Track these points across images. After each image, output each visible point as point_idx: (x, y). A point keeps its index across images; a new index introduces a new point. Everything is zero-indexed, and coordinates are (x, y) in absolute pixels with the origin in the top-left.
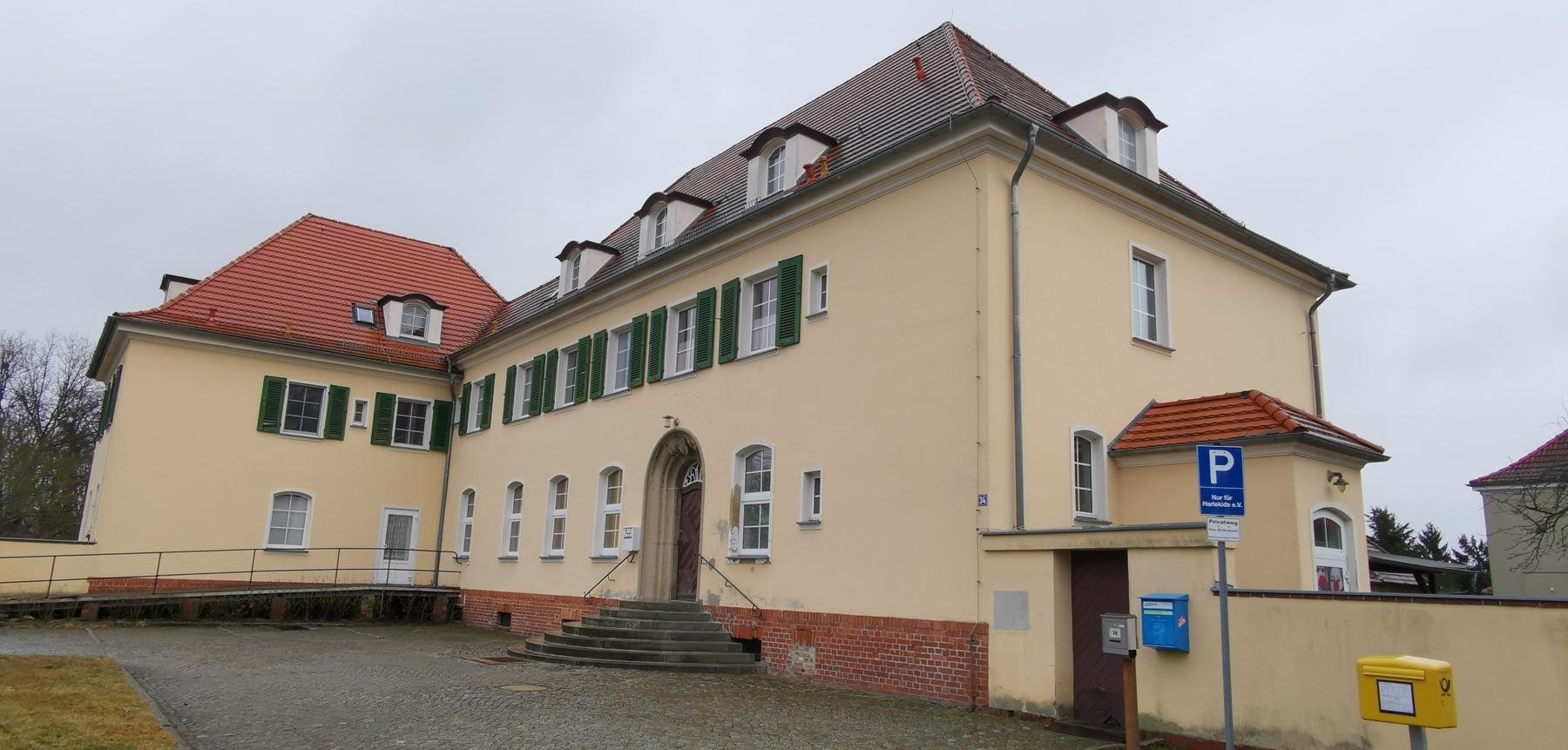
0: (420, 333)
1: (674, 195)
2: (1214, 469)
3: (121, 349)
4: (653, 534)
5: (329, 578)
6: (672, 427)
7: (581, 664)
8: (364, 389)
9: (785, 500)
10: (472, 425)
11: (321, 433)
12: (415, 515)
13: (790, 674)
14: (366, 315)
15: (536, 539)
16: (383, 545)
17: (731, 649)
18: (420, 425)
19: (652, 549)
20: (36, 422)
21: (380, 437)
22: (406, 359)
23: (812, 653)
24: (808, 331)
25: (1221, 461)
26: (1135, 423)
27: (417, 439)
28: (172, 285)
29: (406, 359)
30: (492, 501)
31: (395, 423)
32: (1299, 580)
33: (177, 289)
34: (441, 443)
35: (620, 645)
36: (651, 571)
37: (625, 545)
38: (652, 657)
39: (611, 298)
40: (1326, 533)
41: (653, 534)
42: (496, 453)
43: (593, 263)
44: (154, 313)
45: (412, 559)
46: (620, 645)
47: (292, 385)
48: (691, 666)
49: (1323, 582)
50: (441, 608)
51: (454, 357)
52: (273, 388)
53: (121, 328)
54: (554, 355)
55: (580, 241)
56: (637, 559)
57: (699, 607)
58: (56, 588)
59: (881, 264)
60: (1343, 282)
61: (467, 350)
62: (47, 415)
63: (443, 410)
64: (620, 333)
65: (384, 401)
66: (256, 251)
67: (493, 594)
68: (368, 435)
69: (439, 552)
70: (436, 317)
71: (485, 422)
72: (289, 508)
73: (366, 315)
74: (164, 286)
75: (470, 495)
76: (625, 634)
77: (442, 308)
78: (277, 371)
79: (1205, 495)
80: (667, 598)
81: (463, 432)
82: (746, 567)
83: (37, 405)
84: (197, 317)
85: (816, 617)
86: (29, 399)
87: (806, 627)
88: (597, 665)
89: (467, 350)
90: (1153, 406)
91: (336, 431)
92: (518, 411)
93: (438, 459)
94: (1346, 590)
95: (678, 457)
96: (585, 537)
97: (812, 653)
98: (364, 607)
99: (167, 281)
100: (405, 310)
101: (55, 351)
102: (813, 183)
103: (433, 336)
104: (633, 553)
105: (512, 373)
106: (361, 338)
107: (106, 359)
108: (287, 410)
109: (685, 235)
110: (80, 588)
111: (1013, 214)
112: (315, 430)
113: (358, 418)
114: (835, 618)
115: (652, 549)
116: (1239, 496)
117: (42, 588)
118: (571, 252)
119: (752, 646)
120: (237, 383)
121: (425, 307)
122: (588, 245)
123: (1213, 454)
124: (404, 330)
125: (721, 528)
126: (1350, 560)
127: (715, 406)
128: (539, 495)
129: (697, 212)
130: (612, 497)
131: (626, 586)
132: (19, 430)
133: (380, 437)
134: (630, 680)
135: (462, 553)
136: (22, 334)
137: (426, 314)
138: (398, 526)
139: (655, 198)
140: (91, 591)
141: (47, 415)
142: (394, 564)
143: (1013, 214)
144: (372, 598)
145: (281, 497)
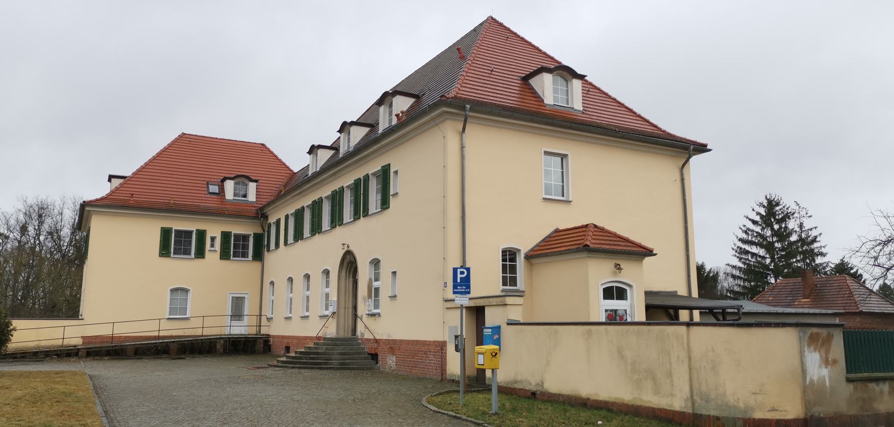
0: (245, 196)
1: (395, 92)
2: (459, 276)
3: (88, 220)
4: (342, 303)
5: (199, 332)
6: (346, 249)
7: (293, 368)
8: (214, 230)
9: (384, 284)
10: (272, 246)
11: (193, 256)
12: (246, 296)
13: (387, 370)
14: (214, 189)
15: (299, 310)
16: (230, 313)
17: (366, 358)
18: (246, 247)
19: (342, 311)
20: (59, 249)
21: (225, 255)
22: (236, 212)
23: (394, 358)
24: (393, 202)
25: (462, 273)
26: (543, 241)
27: (245, 255)
28: (113, 180)
29: (236, 212)
30: (282, 285)
31: (232, 248)
32: (589, 317)
33: (116, 182)
34: (258, 256)
35: (313, 358)
36: (342, 324)
37: (332, 309)
38: (325, 364)
39: (322, 181)
40: (614, 292)
41: (342, 303)
42: (284, 260)
43: (324, 156)
44: (102, 199)
45: (246, 320)
46: (313, 358)
47: (176, 231)
48: (343, 367)
49: (609, 317)
50: (260, 346)
51: (261, 209)
52: (166, 233)
53: (87, 209)
54: (367, 178)
55: (349, 121)
56: (335, 316)
57: (357, 339)
58: (66, 342)
59: (422, 166)
60: (702, 148)
61: (269, 204)
62: (65, 242)
63: (258, 238)
64: (327, 197)
65: (226, 236)
66: (154, 158)
67: (283, 337)
68: (218, 255)
69: (261, 315)
70: (252, 186)
71: (277, 245)
72: (179, 296)
73: (214, 189)
74: (110, 180)
75: (272, 283)
76: (317, 353)
77: (256, 181)
78: (167, 224)
79: (455, 287)
80: (350, 335)
81: (268, 250)
82: (373, 318)
83: (59, 238)
84: (128, 198)
85: (395, 341)
86: (54, 233)
87: (393, 346)
88: (300, 368)
89: (269, 204)
90: (557, 231)
91: (200, 254)
92: (291, 239)
93: (257, 265)
94: (629, 320)
95: (349, 263)
96: (318, 308)
97: (394, 358)
98: (218, 346)
99: (111, 178)
100: (235, 184)
101: (66, 206)
102: (407, 119)
103: (252, 197)
104: (334, 313)
105: (287, 217)
106: (213, 203)
107: (84, 222)
108: (173, 244)
109: (359, 143)
110: (78, 342)
111: (462, 147)
112: (189, 254)
113: (212, 246)
114: (402, 341)
115: (342, 311)
116: (468, 287)
117: (59, 342)
118: (313, 150)
119: (374, 357)
120: (146, 232)
121: (246, 181)
122: (353, 123)
123: (459, 271)
124: (235, 195)
125: (364, 300)
126: (632, 306)
127: (361, 236)
128: (299, 282)
129: (411, 101)
130: (327, 286)
131: (331, 331)
132: (51, 253)
133: (225, 255)
134: (307, 373)
135: (269, 316)
136: (48, 197)
137: (246, 185)
138: (238, 303)
139: (386, 95)
140: (83, 343)
141: (65, 242)
142: (234, 323)
143: (462, 147)
144: (222, 341)
145: (174, 291)
